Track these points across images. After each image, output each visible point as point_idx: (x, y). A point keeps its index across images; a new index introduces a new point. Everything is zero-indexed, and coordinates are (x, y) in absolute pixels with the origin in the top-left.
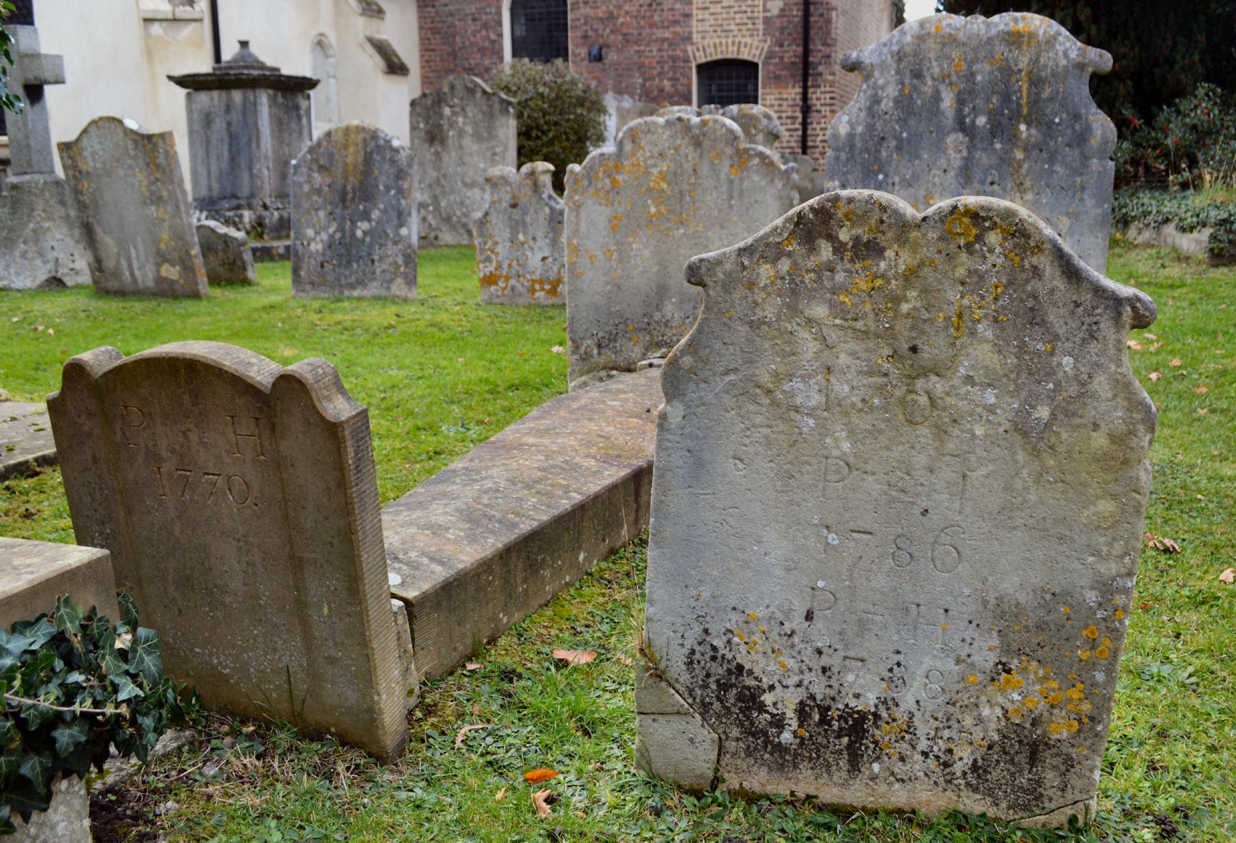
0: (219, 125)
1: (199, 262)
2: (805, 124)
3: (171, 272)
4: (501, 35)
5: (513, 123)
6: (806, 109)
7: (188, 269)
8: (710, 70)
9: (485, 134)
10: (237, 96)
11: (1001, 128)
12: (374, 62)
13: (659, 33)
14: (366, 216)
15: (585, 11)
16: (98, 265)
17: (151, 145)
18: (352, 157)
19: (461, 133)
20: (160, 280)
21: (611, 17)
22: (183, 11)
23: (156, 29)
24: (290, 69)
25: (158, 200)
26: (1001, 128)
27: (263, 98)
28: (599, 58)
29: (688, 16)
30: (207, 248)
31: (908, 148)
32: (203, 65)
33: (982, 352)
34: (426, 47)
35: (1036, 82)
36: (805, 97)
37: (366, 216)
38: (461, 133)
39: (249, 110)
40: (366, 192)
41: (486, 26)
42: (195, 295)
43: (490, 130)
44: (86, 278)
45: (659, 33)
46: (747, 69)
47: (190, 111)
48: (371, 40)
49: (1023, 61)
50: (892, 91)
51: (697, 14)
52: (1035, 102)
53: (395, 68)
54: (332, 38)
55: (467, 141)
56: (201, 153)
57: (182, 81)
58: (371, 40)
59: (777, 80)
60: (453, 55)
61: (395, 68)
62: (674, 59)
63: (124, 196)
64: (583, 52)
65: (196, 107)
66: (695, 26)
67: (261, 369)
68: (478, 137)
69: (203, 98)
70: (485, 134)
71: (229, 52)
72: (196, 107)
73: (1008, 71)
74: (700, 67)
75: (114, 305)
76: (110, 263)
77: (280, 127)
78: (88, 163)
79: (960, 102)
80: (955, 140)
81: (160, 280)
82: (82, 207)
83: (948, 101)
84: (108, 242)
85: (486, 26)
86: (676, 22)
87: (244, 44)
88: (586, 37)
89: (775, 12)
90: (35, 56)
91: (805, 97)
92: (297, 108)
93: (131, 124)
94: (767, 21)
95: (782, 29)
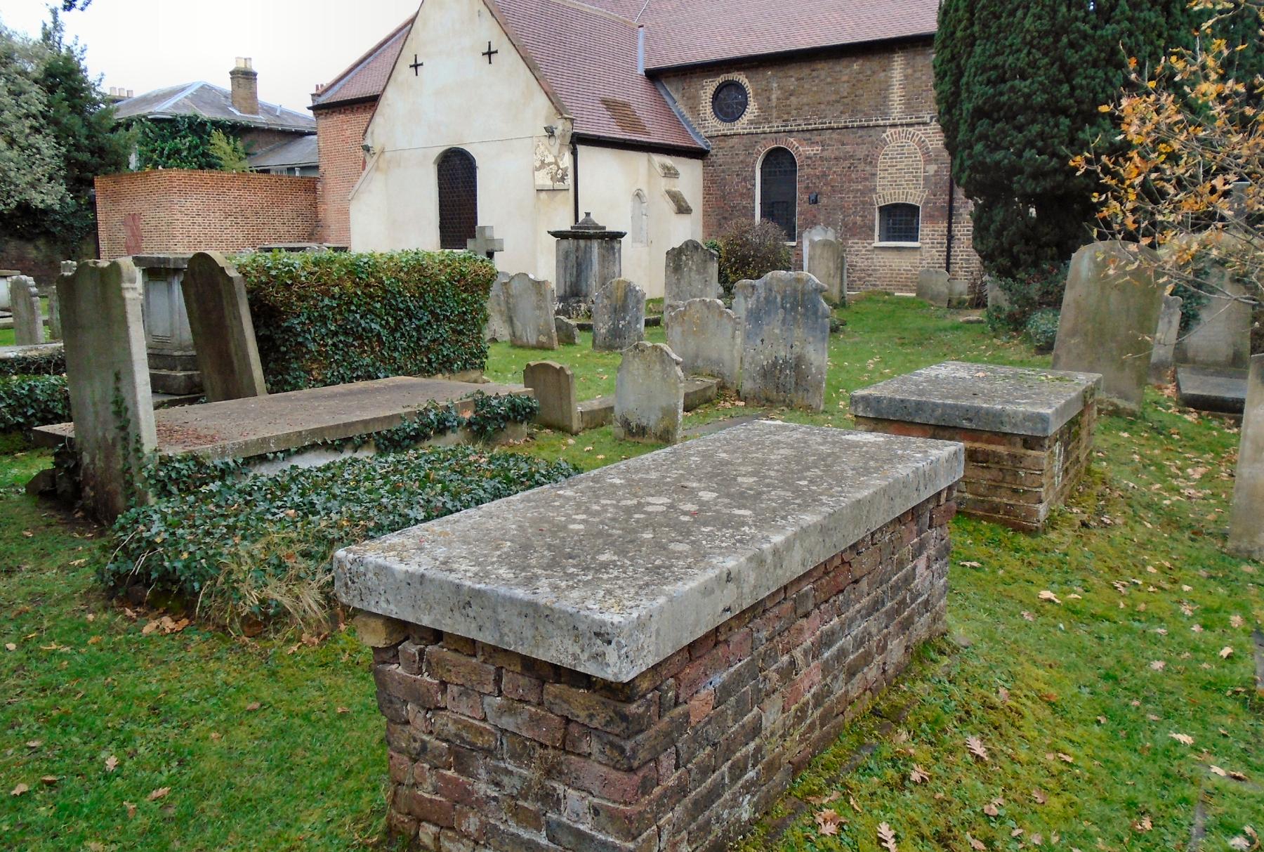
0: (572, 257)
1: (555, 335)
2: (949, 248)
3: (543, 339)
4: (754, 185)
5: (716, 265)
6: (950, 237)
7: (550, 338)
8: (889, 211)
9: (702, 270)
10: (582, 243)
11: (794, 308)
12: (670, 207)
13: (854, 186)
14: (624, 319)
15: (807, 171)
16: (514, 334)
17: (539, 285)
18: (620, 293)
19: (690, 269)
20: (538, 341)
21: (824, 175)
22: (559, 185)
23: (543, 195)
24: (610, 228)
25: (540, 308)
26: (794, 308)
27: (595, 244)
28: (815, 202)
29: (875, 175)
30: (558, 328)
31: (768, 313)
32: (566, 225)
33: (658, 367)
34: (707, 191)
35: (803, 294)
36: (950, 230)
37: (624, 319)
38: (690, 269)
39: (588, 251)
40: (624, 308)
41: (745, 179)
42: (552, 349)
43: (705, 268)
44: (507, 338)
45: (854, 186)
46: (912, 210)
47: (558, 250)
48: (668, 192)
49: (800, 287)
50: (763, 295)
51: (880, 174)
52: (803, 300)
53: (683, 209)
54: (646, 192)
55: (693, 274)
56: (562, 272)
57: (555, 234)
58: (668, 192)
59: (931, 218)
60: (724, 197)
61: (683, 209)
62: (864, 203)
63: (526, 306)
64: (806, 197)
65: (561, 248)
66: (878, 182)
67: (558, 366)
68: (698, 272)
69: (565, 242)
70: (702, 270)
71: (582, 217)
72: (561, 248)
73: (795, 290)
74: (881, 209)
75: (518, 351)
76: (518, 334)
77: (603, 259)
78: (513, 291)
79: (782, 299)
80: (781, 311)
81: (538, 341)
82: (509, 309)
83: (779, 299)
84: (518, 324)
85: (745, 179)
86: (866, 179)
87: (588, 214)
88: (807, 187)
89: (932, 172)
90: (493, 240)
91: (950, 230)
92: (613, 248)
93: (531, 276)
94: (926, 178)
95: (936, 184)
